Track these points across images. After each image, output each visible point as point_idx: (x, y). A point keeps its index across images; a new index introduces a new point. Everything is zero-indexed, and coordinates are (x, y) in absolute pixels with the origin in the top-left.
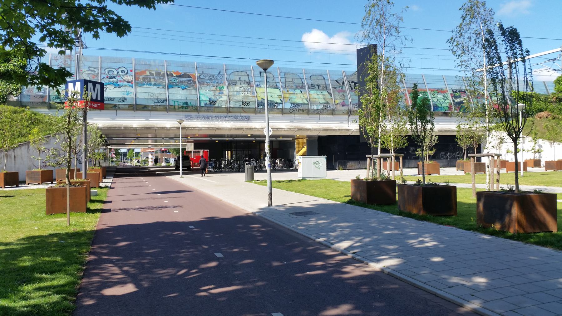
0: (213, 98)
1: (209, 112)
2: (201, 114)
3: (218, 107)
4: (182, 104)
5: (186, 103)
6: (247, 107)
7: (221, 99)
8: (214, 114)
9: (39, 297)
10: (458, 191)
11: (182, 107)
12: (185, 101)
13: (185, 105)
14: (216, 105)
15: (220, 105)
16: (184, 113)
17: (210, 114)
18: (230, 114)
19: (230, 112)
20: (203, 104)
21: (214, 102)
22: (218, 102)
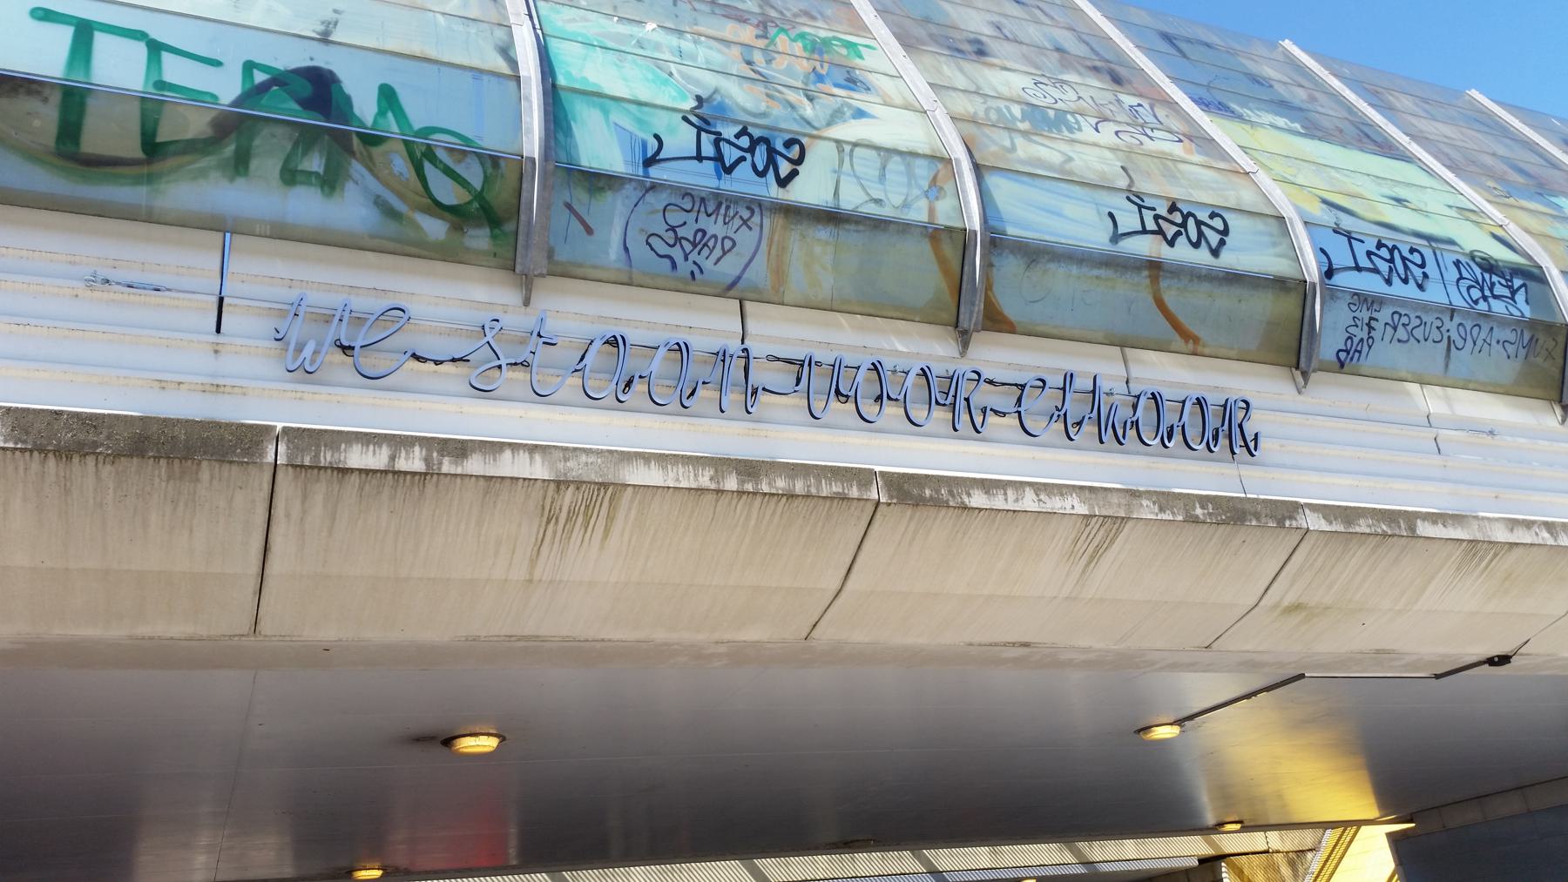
0: (743, 98)
1: (693, 283)
2: (574, 312)
3: (832, 217)
4: (227, 88)
5: (319, 88)
6: (1202, 257)
7: (849, 131)
8: (778, 332)
9: (304, 512)
10: (91, 103)
11: (232, 138)
12: (291, 58)
13: (288, 109)
14: (810, 189)
15: (852, 199)
16: (263, 275)
17: (710, 325)
18: (998, 357)
19: (996, 321)
20: (600, 146)
21: (779, 153)
22: (819, 159)
